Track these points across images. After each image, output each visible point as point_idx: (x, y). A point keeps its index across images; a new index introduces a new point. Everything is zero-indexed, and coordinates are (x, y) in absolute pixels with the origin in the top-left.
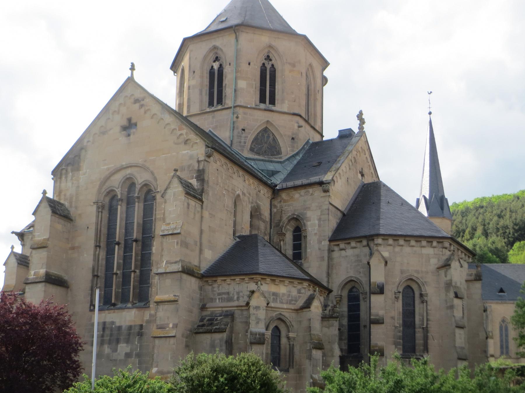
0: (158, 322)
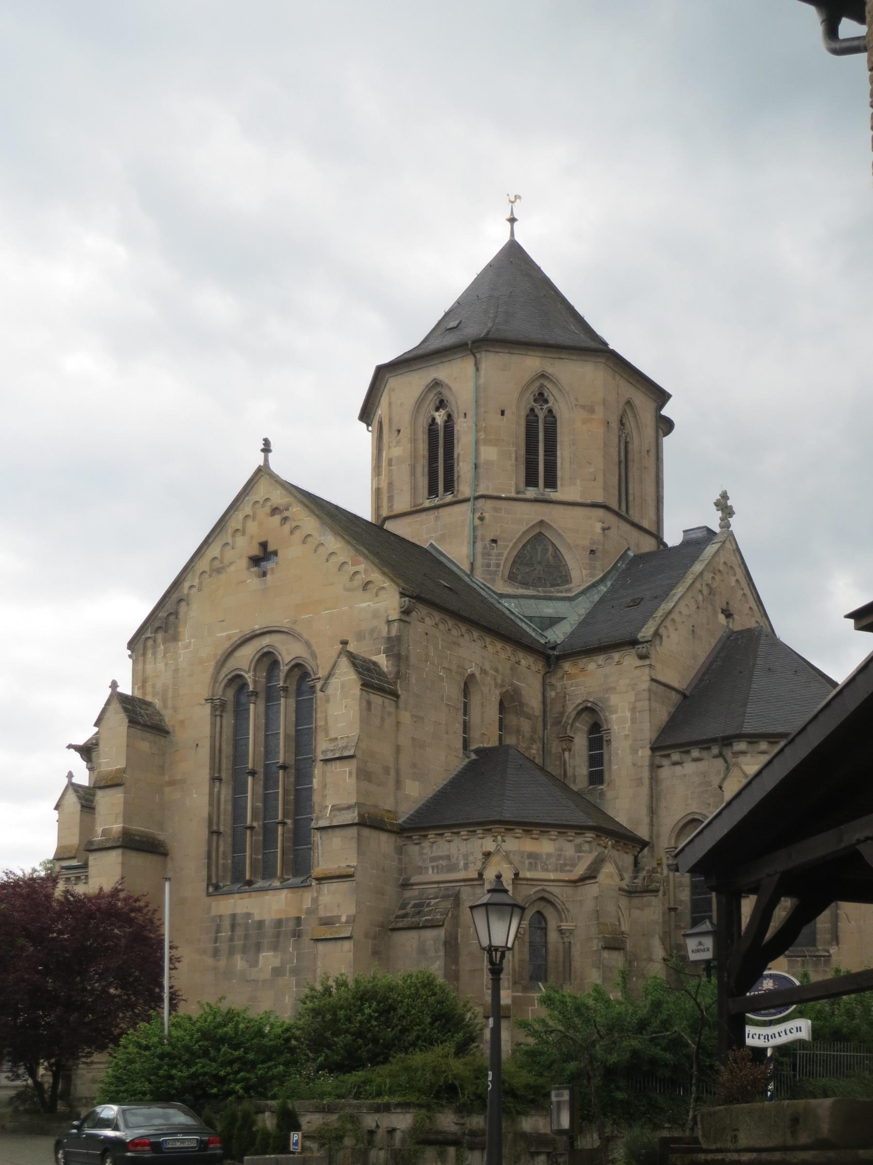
0: (322, 914)
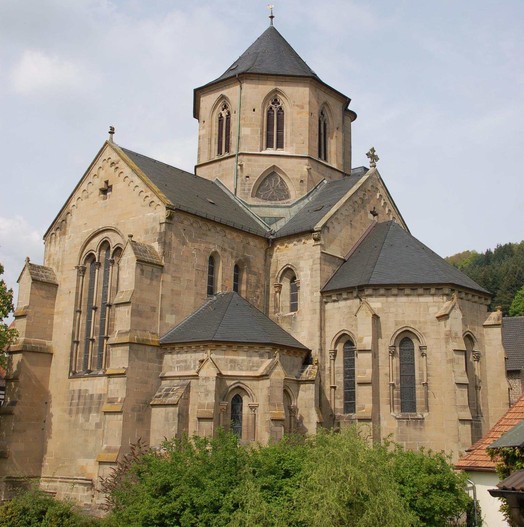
0: (110, 396)
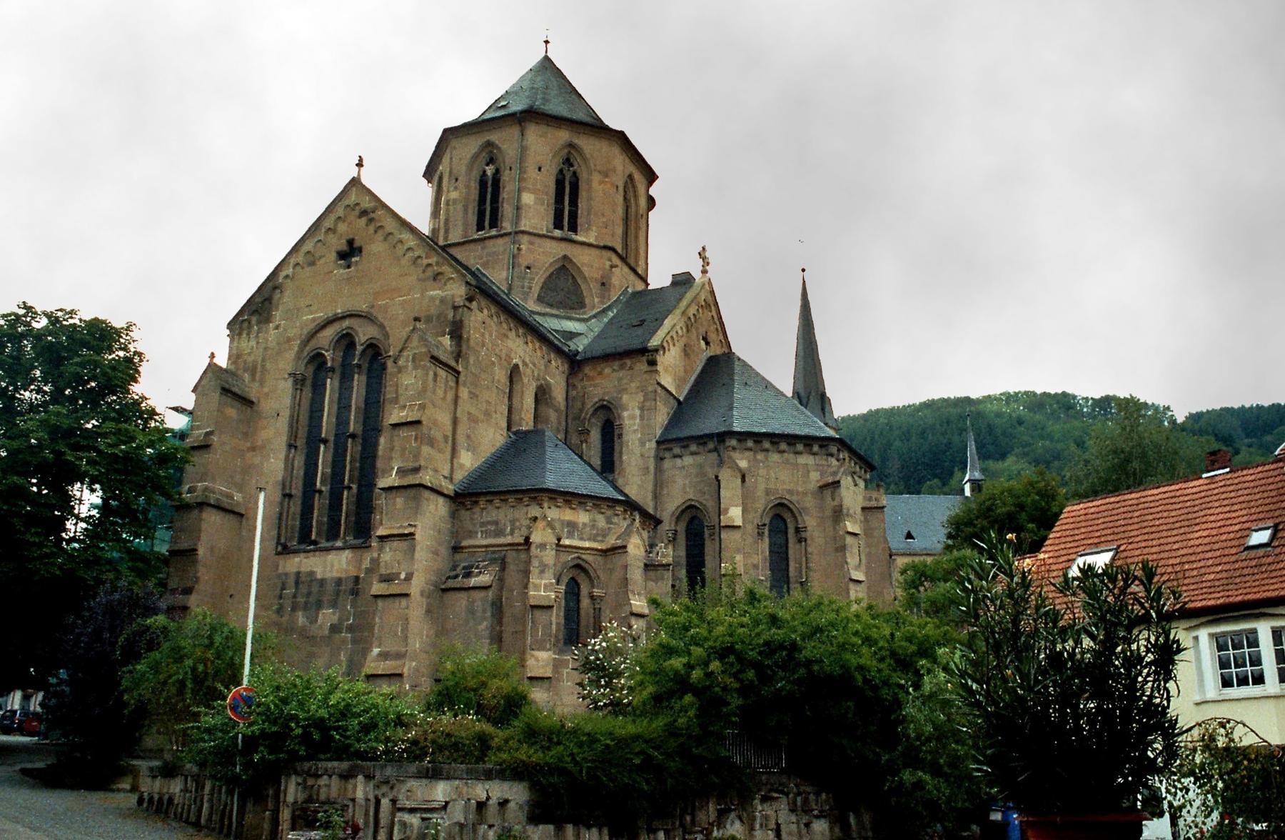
0: (383, 571)
